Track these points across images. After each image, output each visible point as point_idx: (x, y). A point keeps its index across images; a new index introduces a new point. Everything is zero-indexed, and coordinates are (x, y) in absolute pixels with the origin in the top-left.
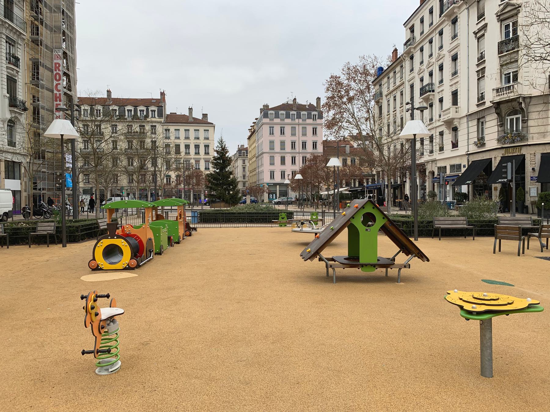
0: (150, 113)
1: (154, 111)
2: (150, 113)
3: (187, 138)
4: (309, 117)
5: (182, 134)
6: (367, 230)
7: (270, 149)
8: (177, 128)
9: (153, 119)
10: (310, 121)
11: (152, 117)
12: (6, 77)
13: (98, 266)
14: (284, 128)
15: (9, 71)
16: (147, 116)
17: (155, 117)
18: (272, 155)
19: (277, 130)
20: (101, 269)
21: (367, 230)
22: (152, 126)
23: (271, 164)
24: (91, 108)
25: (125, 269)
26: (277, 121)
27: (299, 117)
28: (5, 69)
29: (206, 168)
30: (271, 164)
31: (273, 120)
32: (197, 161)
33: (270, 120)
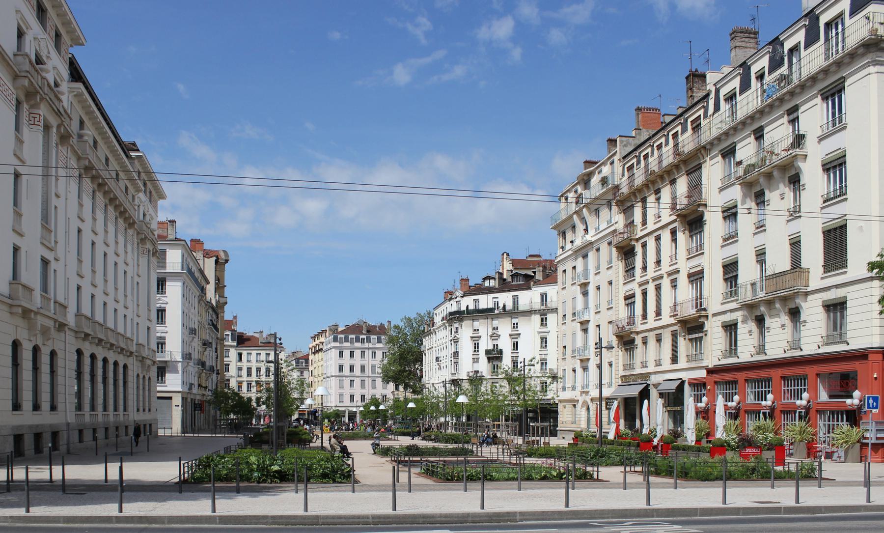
10: (347, 344)
19: (347, 353)
27: (369, 341)
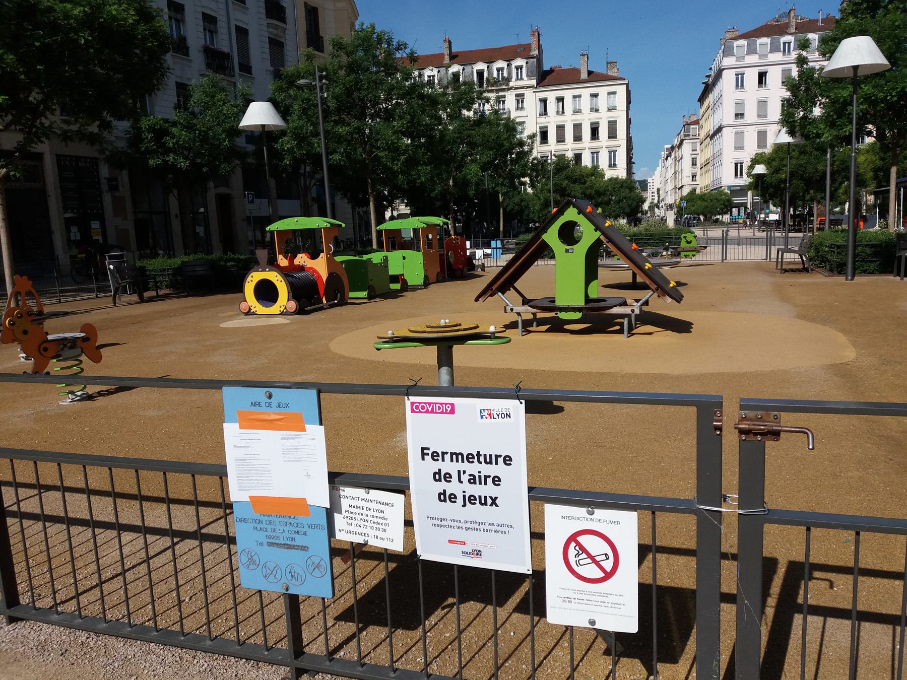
0: (514, 71)
1: (521, 67)
2: (514, 71)
3: (577, 111)
4: (774, 49)
5: (585, 103)
6: (567, 251)
7: (759, 116)
8: (594, 91)
9: (520, 83)
11: (517, 79)
12: (267, 40)
13: (250, 309)
14: (743, 74)
15: (271, 30)
16: (508, 80)
17: (522, 79)
18: (739, 129)
20: (254, 314)
21: (567, 251)
22: (517, 95)
23: (737, 148)
24: (508, 65)
25: (282, 314)
26: (753, 59)
28: (265, 28)
29: (610, 166)
30: (737, 148)
31: (766, 56)
32: (595, 154)
33: (761, 57)
